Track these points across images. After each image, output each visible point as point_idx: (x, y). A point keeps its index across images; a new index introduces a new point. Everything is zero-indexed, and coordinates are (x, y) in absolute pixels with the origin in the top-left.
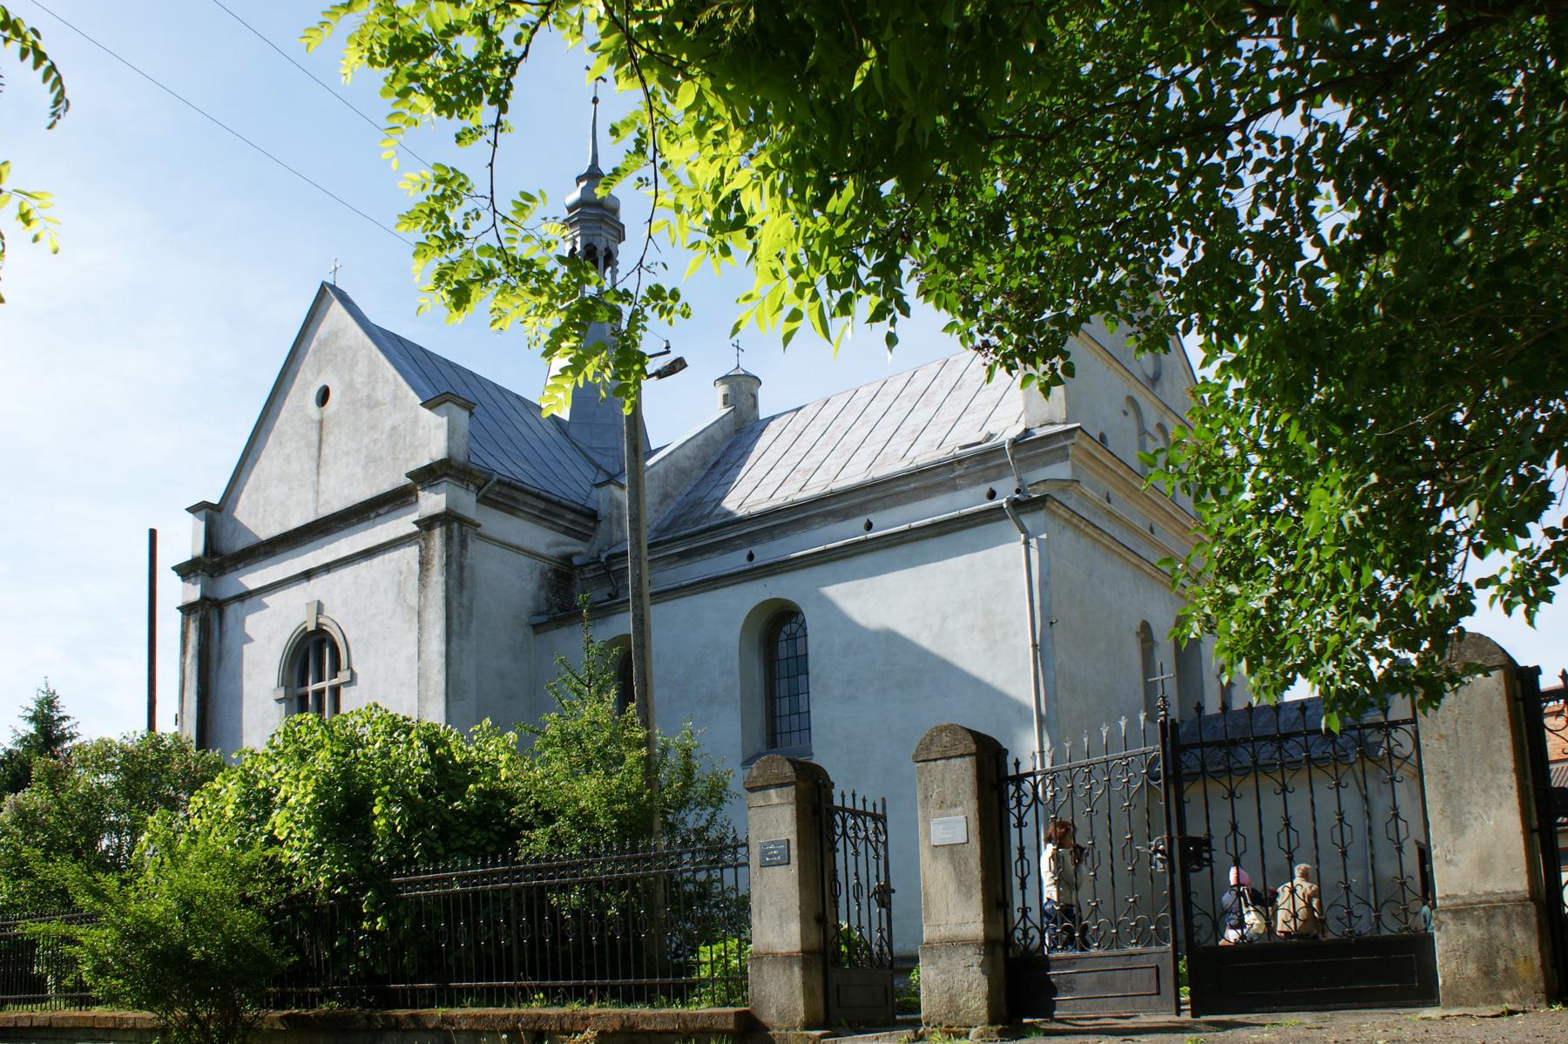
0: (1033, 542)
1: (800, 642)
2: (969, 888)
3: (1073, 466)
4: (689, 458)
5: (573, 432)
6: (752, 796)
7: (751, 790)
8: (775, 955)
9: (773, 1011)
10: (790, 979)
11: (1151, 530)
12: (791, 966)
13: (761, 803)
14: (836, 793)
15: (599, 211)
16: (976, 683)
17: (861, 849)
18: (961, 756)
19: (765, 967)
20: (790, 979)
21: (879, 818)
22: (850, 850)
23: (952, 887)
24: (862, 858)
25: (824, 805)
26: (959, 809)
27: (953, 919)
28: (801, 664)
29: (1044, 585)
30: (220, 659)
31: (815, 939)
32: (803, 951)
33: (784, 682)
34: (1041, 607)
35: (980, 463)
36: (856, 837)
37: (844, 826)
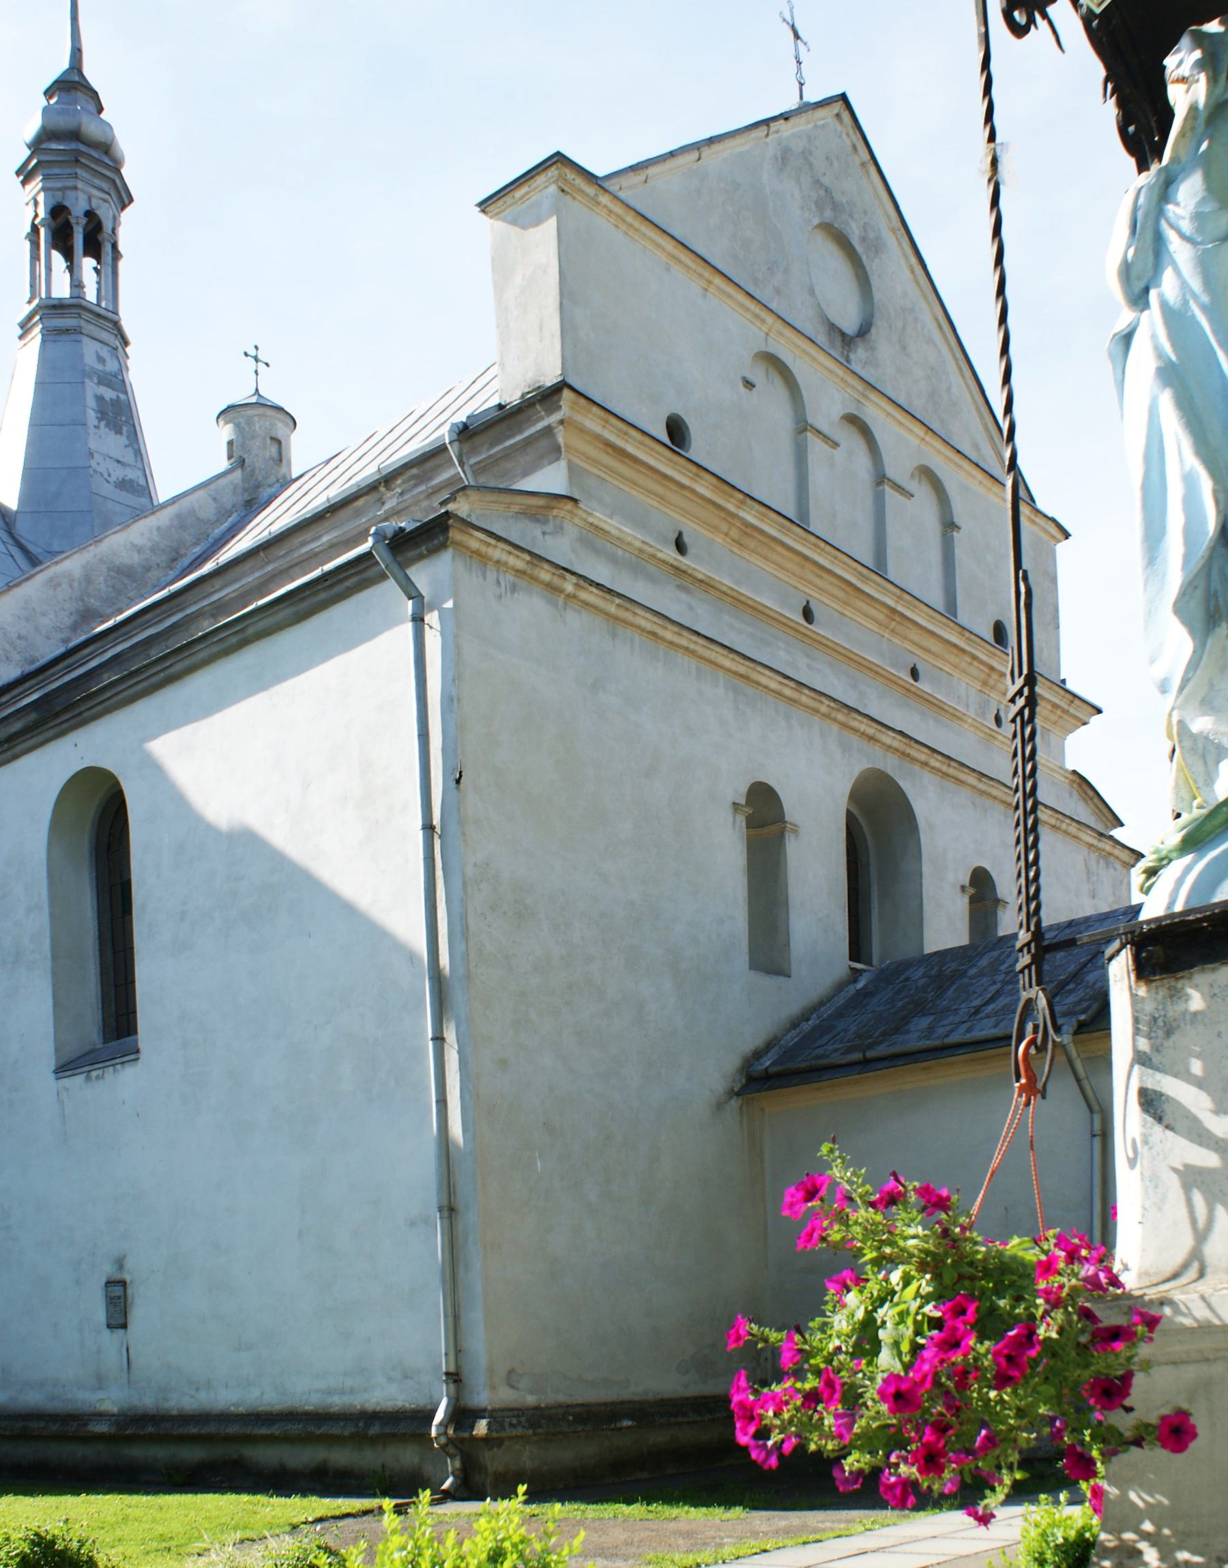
0: (432, 618)
3: (572, 468)
4: (139, 550)
5: (22, 528)
11: (808, 614)
15: (73, 146)
16: (349, 911)
30: (819, 1089)
35: (421, 479)
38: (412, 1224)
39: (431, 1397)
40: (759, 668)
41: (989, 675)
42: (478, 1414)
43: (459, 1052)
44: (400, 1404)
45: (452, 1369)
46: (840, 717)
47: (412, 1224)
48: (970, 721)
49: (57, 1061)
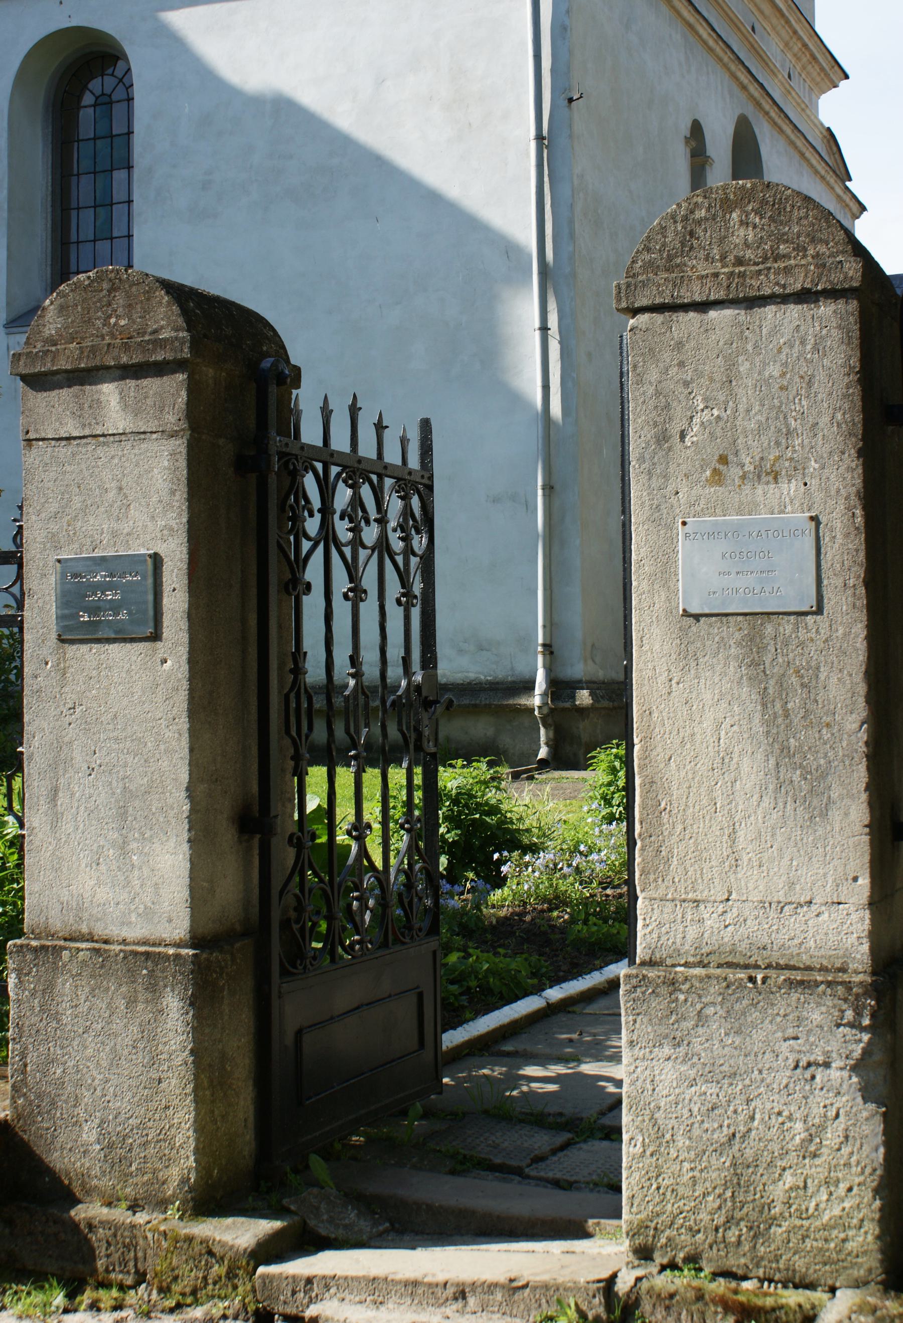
1: (118, 110)
2: (816, 781)
6: (41, 400)
7: (38, 382)
8: (99, 945)
9: (89, 1134)
10: (149, 1035)
12: (153, 988)
13: (71, 428)
14: (307, 399)
17: (369, 580)
18: (805, 296)
19: (65, 986)
20: (149, 1035)
21: (419, 485)
22: (341, 582)
23: (751, 768)
24: (369, 609)
25: (276, 441)
26: (791, 488)
27: (753, 884)
28: (117, 150)
29: (560, 31)
31: (231, 891)
32: (197, 940)
33: (86, 182)
34: (553, 71)
36: (357, 543)
37: (326, 510)
38: (496, 500)
39: (512, 669)
40: (701, 20)
41: (791, 38)
42: (577, 685)
43: (560, 342)
44: (472, 676)
45: (548, 642)
46: (733, 67)
47: (496, 500)
48: (780, 77)
49: (8, 315)
